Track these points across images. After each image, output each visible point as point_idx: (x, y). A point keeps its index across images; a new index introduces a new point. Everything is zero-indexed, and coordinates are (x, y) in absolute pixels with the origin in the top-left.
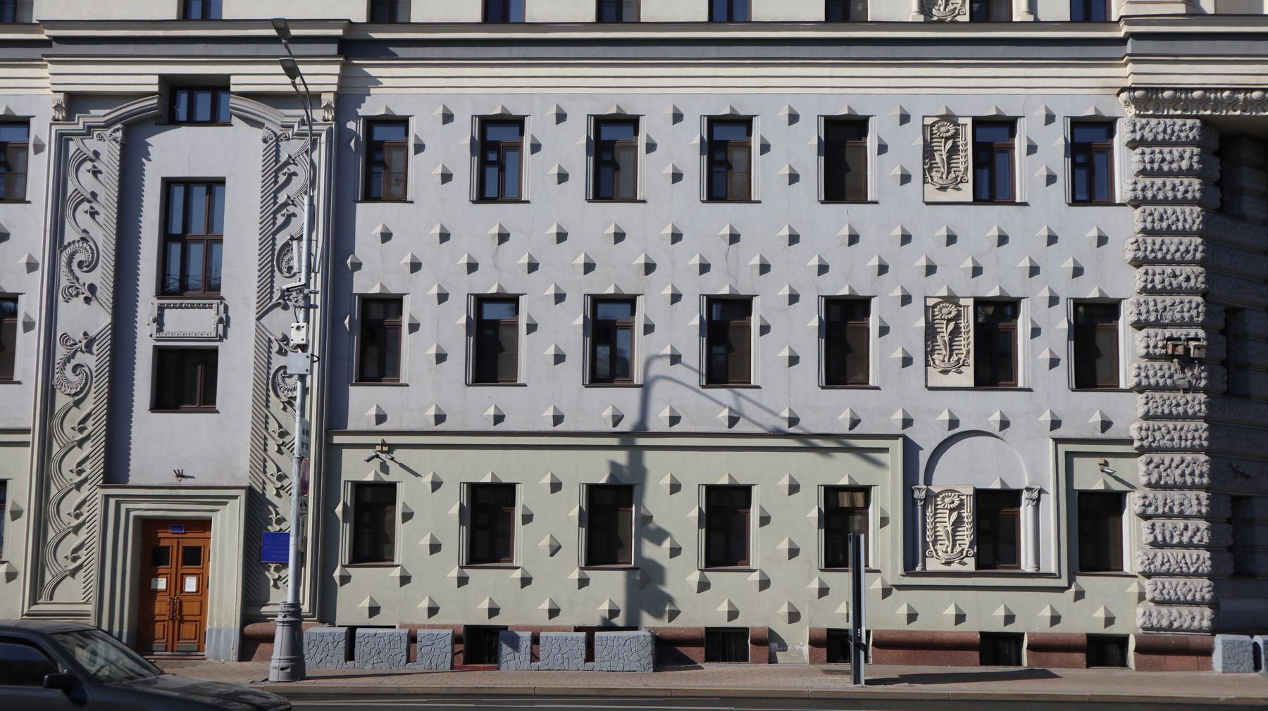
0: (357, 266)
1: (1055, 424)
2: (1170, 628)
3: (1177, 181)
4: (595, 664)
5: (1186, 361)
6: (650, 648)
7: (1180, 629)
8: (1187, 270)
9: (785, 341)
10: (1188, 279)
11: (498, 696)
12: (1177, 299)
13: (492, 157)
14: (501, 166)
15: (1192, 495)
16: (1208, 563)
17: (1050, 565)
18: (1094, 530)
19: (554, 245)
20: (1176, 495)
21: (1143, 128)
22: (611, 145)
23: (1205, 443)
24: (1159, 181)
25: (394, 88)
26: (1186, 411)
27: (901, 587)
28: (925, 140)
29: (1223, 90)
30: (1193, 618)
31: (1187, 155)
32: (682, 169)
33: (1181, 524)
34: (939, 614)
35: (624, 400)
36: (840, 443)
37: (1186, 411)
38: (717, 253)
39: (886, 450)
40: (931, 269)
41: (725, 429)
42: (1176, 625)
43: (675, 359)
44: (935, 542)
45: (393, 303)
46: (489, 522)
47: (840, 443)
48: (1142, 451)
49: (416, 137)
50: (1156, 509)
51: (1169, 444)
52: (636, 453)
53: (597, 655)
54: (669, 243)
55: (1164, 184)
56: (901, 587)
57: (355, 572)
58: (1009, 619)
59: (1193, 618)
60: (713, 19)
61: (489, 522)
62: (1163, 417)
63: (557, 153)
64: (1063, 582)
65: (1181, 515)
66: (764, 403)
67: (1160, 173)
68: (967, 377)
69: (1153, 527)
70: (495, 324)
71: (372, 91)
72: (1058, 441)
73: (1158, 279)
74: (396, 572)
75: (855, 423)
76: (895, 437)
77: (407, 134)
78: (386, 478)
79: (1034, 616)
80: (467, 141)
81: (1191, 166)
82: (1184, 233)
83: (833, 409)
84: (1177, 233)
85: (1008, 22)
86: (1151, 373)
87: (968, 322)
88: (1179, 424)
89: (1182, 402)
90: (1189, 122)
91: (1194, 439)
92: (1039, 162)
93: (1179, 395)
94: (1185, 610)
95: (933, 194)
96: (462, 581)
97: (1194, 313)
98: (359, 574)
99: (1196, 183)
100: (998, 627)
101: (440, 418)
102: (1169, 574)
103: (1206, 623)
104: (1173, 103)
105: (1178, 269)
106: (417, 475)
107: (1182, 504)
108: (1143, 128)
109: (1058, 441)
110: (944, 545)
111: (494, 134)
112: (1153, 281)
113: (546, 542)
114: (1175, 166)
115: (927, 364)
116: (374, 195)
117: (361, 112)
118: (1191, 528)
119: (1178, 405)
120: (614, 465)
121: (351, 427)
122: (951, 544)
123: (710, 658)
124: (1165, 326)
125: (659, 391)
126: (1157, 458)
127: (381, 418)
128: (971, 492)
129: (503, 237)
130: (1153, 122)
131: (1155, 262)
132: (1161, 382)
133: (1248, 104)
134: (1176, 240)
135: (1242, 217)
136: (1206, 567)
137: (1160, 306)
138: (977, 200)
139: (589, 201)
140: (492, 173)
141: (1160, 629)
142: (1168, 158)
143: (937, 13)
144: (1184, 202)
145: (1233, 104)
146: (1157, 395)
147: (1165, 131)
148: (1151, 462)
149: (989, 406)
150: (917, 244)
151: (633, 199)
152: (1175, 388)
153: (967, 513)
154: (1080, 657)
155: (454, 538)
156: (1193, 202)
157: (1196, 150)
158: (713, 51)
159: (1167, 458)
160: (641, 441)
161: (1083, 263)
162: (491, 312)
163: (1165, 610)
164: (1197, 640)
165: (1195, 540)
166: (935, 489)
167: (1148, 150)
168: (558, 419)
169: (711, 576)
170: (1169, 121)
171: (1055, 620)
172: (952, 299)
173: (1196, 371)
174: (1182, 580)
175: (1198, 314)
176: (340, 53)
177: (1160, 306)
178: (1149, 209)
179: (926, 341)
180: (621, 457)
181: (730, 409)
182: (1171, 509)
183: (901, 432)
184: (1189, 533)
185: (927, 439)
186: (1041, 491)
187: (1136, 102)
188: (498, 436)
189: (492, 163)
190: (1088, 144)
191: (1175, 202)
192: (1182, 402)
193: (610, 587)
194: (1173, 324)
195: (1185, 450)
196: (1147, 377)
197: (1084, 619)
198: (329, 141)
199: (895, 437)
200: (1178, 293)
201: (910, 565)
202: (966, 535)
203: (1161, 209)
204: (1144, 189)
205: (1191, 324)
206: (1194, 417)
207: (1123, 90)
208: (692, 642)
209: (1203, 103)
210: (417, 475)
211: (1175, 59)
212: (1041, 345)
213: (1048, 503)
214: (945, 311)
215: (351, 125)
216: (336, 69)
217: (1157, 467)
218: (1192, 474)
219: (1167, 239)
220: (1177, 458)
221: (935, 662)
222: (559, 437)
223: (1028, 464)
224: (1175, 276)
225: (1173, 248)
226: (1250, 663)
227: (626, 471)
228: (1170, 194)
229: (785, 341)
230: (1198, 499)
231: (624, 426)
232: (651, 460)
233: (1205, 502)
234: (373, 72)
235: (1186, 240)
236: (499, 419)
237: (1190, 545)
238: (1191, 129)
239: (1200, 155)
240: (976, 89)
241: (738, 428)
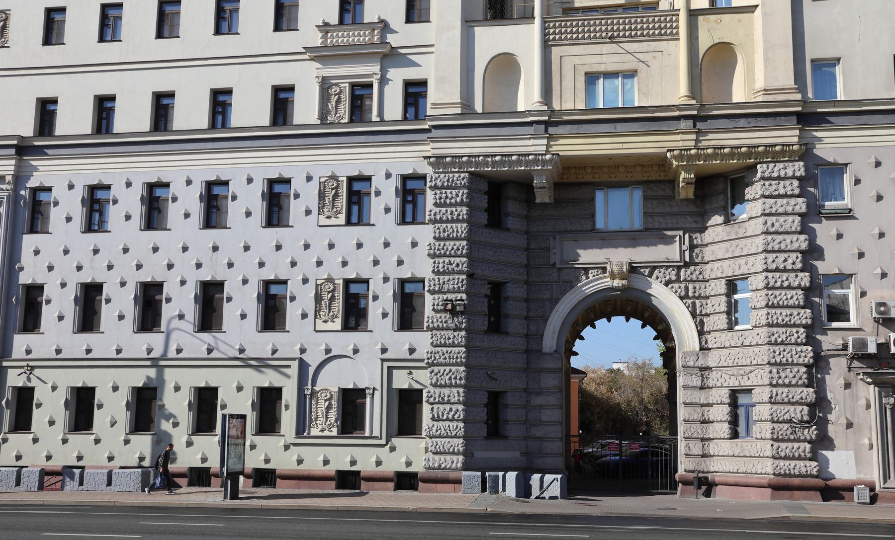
0: (22, 269)
1: (384, 351)
2: (439, 468)
3: (454, 209)
4: (112, 488)
5: (453, 312)
6: (140, 479)
7: (445, 469)
8: (457, 260)
9: (240, 304)
10: (458, 265)
11: (25, 505)
12: (451, 277)
13: (410, 198)
14: (414, 203)
15: (455, 390)
16: (463, 430)
17: (376, 433)
18: (406, 412)
19: (124, 255)
20: (446, 391)
21: (436, 179)
23: (464, 360)
24: (443, 210)
25: (46, 172)
26: (453, 342)
27: (295, 445)
28: (320, 190)
29: (479, 156)
30: (453, 462)
31: (460, 194)
33: (448, 407)
34: (314, 460)
35: (154, 340)
36: (261, 364)
37: (453, 342)
39: (289, 367)
40: (319, 263)
41: (206, 356)
42: (443, 466)
43: (181, 317)
44: (316, 419)
45: (40, 288)
46: (82, 408)
47: (261, 364)
48: (430, 365)
50: (435, 399)
51: (443, 361)
52: (161, 369)
53: (113, 482)
54: (182, 254)
55: (447, 211)
56: (295, 445)
57: (11, 437)
58: (353, 463)
59: (453, 462)
60: (213, 125)
61: (82, 408)
62: (441, 345)
63: (186, 202)
64: (383, 442)
65: (449, 402)
66: (227, 341)
67: (445, 205)
68: (338, 324)
69: (432, 409)
70: (411, 295)
71: (34, 173)
72: (383, 360)
73: (441, 265)
74: (31, 436)
75: (274, 351)
76: (294, 359)
78: (29, 385)
79: (366, 460)
81: (462, 199)
82: (457, 239)
83: (263, 344)
84: (453, 239)
85: (370, 122)
86: (435, 320)
87: (340, 294)
88: (450, 350)
89: (452, 336)
90: (462, 175)
91: (457, 358)
92: (384, 199)
93: (450, 333)
94: (448, 457)
95: (323, 221)
96: (127, 442)
97: (460, 285)
98: (260, 440)
99: (465, 210)
100: (347, 467)
101: (58, 351)
102: (440, 436)
103: (459, 465)
104: (453, 164)
105: (452, 260)
106: (45, 383)
107: (449, 396)
108: (436, 179)
109: (383, 360)
110: (321, 420)
111: (410, 185)
112: (438, 267)
113: (108, 419)
114: (453, 200)
115: (316, 318)
116: (214, 224)
117: (28, 185)
118: (454, 410)
119: (449, 338)
120: (148, 378)
121: (13, 357)
122: (325, 420)
123: (190, 484)
124: (445, 293)
125: (174, 336)
126: (436, 369)
127: (28, 352)
128: (336, 390)
129: (96, 251)
130: (442, 175)
131: (440, 256)
132: (440, 325)
133: (494, 164)
134: (452, 243)
135: (508, 229)
136: (461, 432)
137: (441, 281)
138: (349, 223)
140: (409, 207)
141: (434, 469)
142: (450, 196)
143: (330, 119)
144: (458, 221)
145: (486, 164)
146: (438, 333)
147: (448, 181)
148: (433, 371)
149: (346, 341)
150: (315, 249)
152: (448, 329)
153: (334, 403)
154: (391, 485)
155: (62, 416)
156: (463, 221)
157: (466, 191)
158: (209, 145)
159: (442, 369)
160: (162, 363)
161: (403, 258)
162: (409, 288)
163: (437, 457)
164: (453, 475)
165: (456, 417)
166: (317, 389)
167: (438, 192)
168: (119, 351)
169: (194, 438)
170: (451, 175)
171: (379, 463)
172: (330, 280)
173: (460, 319)
174: (447, 440)
175: (462, 285)
176: (17, 153)
177: (441, 281)
178: (437, 225)
179: (316, 304)
180: (152, 373)
181: (209, 345)
182: (443, 399)
183: (299, 356)
184: (452, 413)
185: (313, 359)
186: (374, 389)
187: (430, 164)
188: (88, 361)
189: (409, 202)
190: (410, 191)
191: (453, 221)
192: (452, 336)
193: (143, 444)
194: (449, 292)
195: (453, 365)
196: (432, 322)
197: (394, 463)
198: (8, 201)
199: (294, 359)
200: (453, 274)
201: (300, 433)
202: (333, 415)
203: (444, 225)
204: (435, 214)
205: (459, 292)
206: (459, 345)
207: (425, 158)
208: (181, 475)
209: (469, 164)
210: (45, 383)
211: (454, 139)
212: (381, 304)
213: (377, 394)
214: (327, 287)
215: (22, 192)
216: (13, 162)
217: (436, 374)
218: (456, 378)
219: (447, 243)
220: (448, 369)
221: (310, 487)
222: (119, 361)
223: (364, 373)
224: (450, 264)
225: (450, 248)
226: (479, 488)
227: (155, 382)
228: (450, 217)
229: (240, 304)
230: (458, 392)
231: (155, 354)
232: (169, 374)
233: (462, 395)
234: (34, 163)
235: (458, 243)
236: (88, 351)
237: (453, 420)
238: (463, 179)
239: (468, 194)
240: (346, 161)
241: (212, 355)
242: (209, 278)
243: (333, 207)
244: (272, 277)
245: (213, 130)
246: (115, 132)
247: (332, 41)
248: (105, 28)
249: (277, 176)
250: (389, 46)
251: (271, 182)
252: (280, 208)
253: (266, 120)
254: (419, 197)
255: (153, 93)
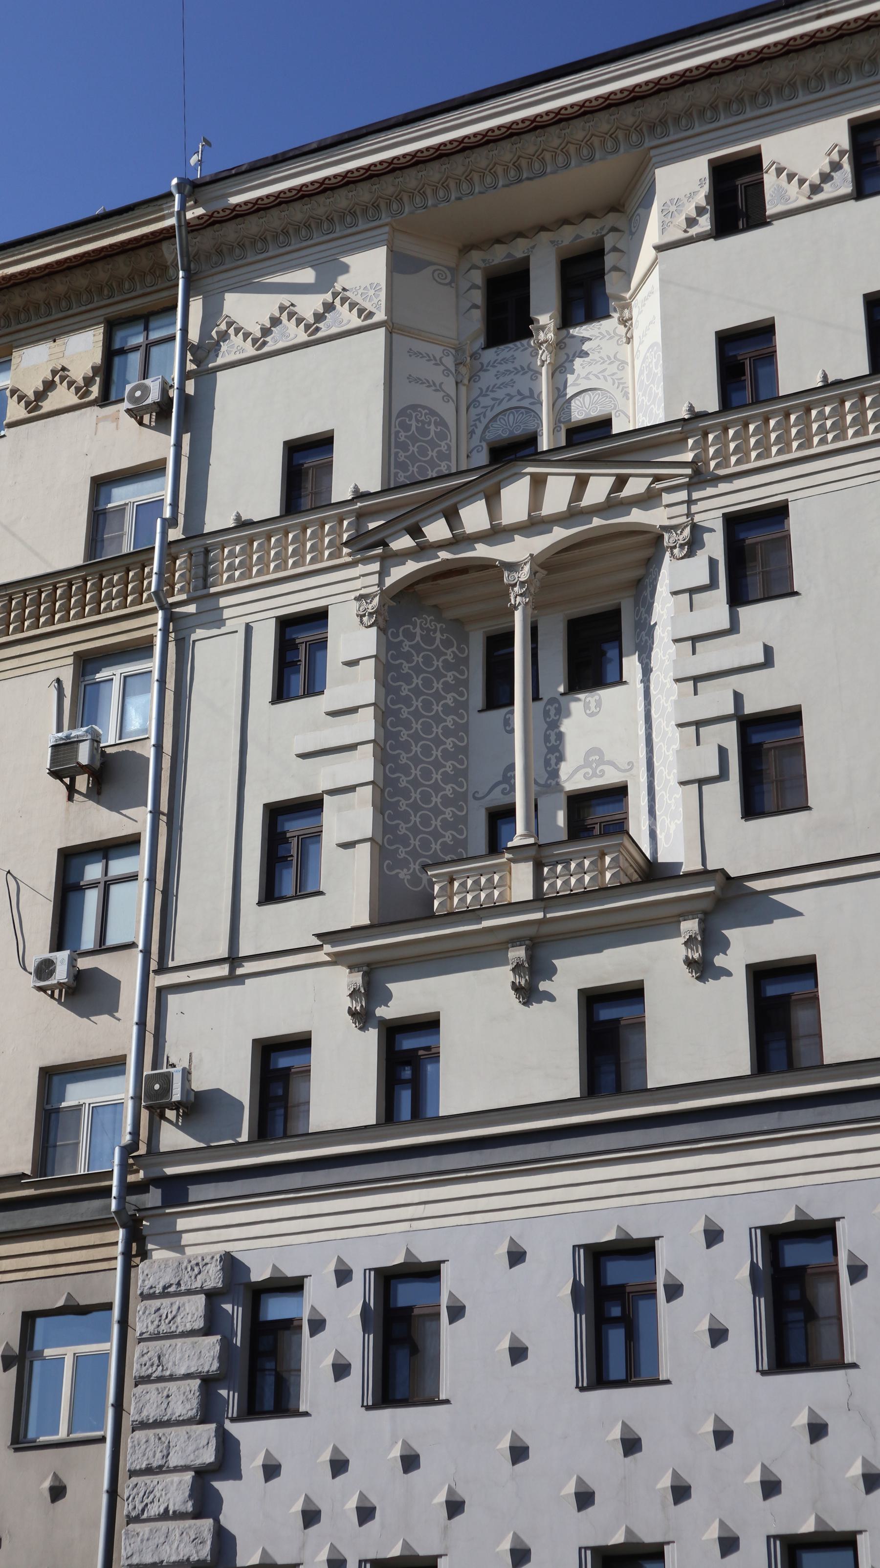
22: (799, 1273)
32: (725, 1321)
38: (793, 1459)
49: (851, 1255)
60: (388, 1113)
77: (835, 1253)
80: (745, 1271)
129: (817, 1430)
139: (764, 1373)
140: (616, 1337)
151: (839, 1364)
189: (615, 1321)
242: (618, 1538)
243: (199, 1358)
244: (808, 1526)
245: (392, 1129)
246: (162, 1150)
247: (463, 900)
248: (73, 897)
249: (611, 1236)
250: (719, 877)
251: (774, 1238)
252: (811, 1315)
253: (740, 1062)
254: (643, 1305)
255: (255, 1041)
